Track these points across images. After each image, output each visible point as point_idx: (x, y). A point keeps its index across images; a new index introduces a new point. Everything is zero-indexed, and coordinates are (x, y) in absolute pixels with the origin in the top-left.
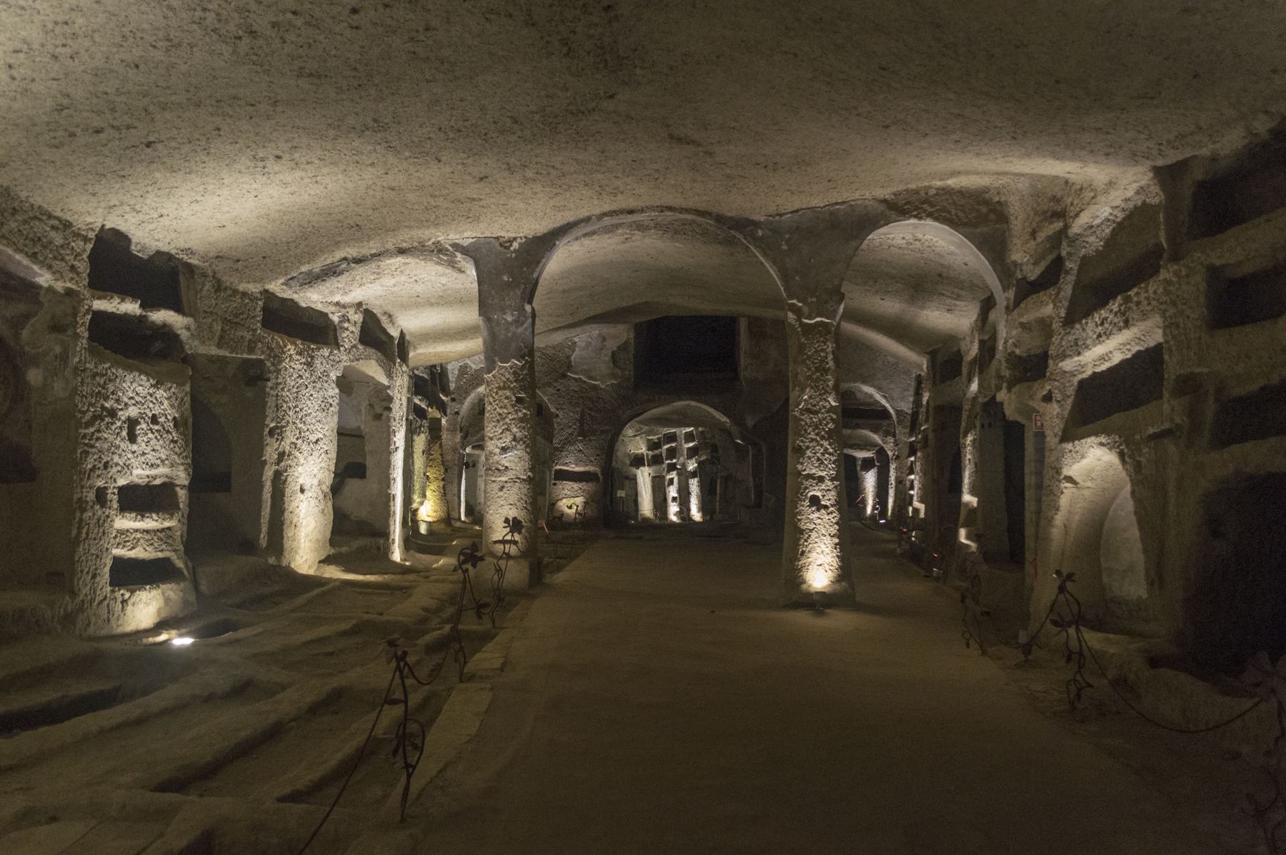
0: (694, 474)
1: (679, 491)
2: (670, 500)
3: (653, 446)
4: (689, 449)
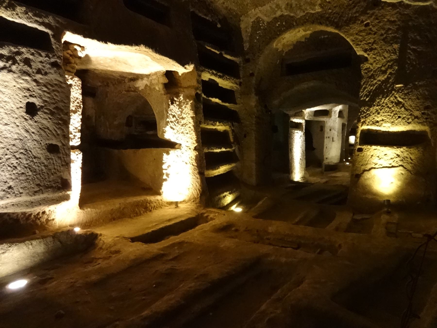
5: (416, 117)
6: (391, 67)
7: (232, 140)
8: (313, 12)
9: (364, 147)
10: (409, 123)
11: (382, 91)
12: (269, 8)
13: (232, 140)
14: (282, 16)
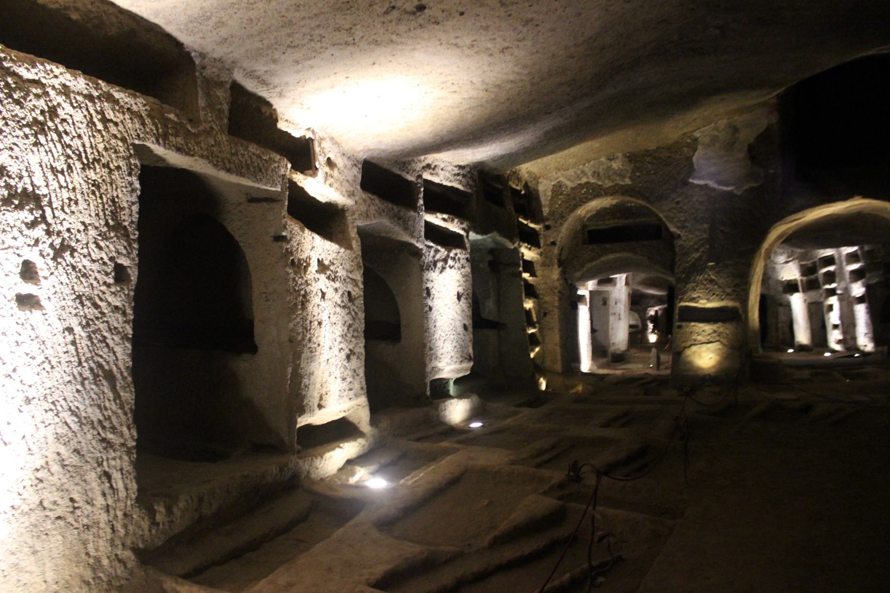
0: (860, 300)
1: (841, 318)
2: (829, 328)
3: (808, 270)
4: (853, 272)
5: (728, 294)
6: (702, 245)
7: (535, 320)
8: (621, 183)
9: (684, 324)
10: (723, 300)
11: (696, 268)
12: (573, 173)
13: (535, 320)
14: (587, 183)
